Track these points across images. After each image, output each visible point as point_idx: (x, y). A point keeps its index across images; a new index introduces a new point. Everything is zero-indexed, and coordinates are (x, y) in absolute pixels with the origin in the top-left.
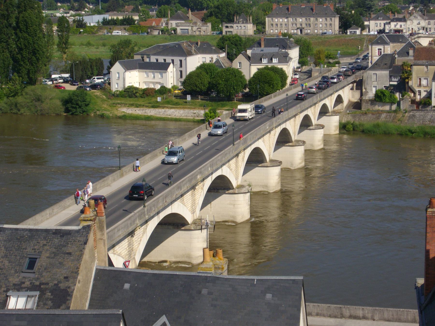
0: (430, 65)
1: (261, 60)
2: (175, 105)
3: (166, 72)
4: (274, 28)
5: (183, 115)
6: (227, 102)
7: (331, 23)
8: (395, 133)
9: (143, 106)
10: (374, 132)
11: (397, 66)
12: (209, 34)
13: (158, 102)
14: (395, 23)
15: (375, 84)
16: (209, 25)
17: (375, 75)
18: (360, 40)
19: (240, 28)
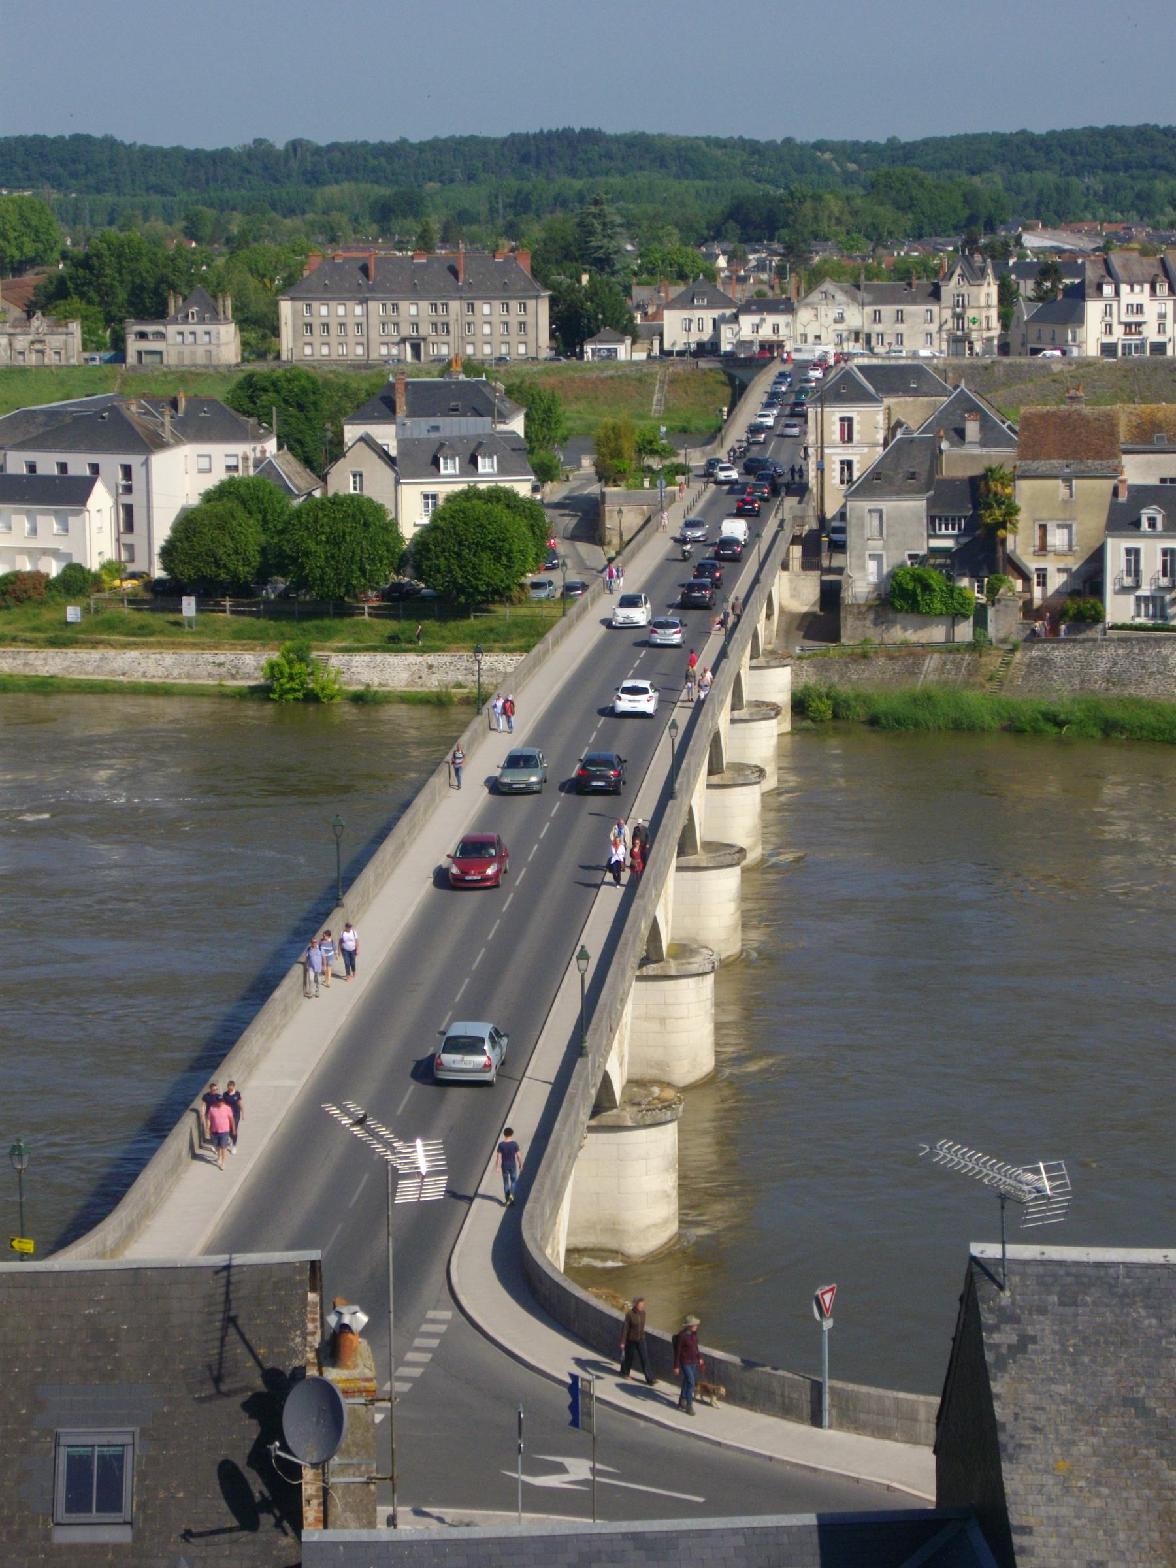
0: (1078, 477)
1: (435, 462)
2: (139, 635)
3: (80, 513)
4: (317, 339)
5: (176, 673)
6: (337, 621)
7: (522, 319)
8: (995, 725)
9: (14, 639)
10: (917, 724)
11: (951, 482)
12: (73, 361)
13: (67, 624)
14: (755, 319)
15: (876, 546)
16: (75, 327)
17: (876, 515)
18: (640, 380)
19: (191, 338)
